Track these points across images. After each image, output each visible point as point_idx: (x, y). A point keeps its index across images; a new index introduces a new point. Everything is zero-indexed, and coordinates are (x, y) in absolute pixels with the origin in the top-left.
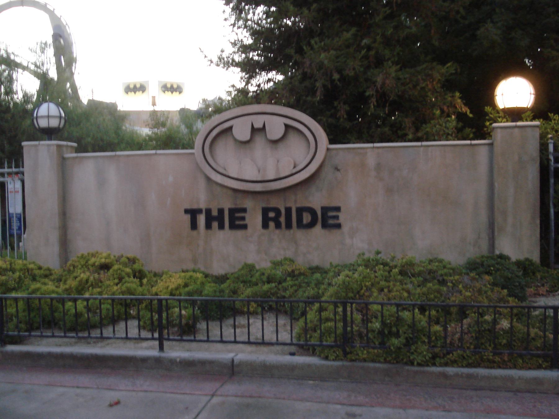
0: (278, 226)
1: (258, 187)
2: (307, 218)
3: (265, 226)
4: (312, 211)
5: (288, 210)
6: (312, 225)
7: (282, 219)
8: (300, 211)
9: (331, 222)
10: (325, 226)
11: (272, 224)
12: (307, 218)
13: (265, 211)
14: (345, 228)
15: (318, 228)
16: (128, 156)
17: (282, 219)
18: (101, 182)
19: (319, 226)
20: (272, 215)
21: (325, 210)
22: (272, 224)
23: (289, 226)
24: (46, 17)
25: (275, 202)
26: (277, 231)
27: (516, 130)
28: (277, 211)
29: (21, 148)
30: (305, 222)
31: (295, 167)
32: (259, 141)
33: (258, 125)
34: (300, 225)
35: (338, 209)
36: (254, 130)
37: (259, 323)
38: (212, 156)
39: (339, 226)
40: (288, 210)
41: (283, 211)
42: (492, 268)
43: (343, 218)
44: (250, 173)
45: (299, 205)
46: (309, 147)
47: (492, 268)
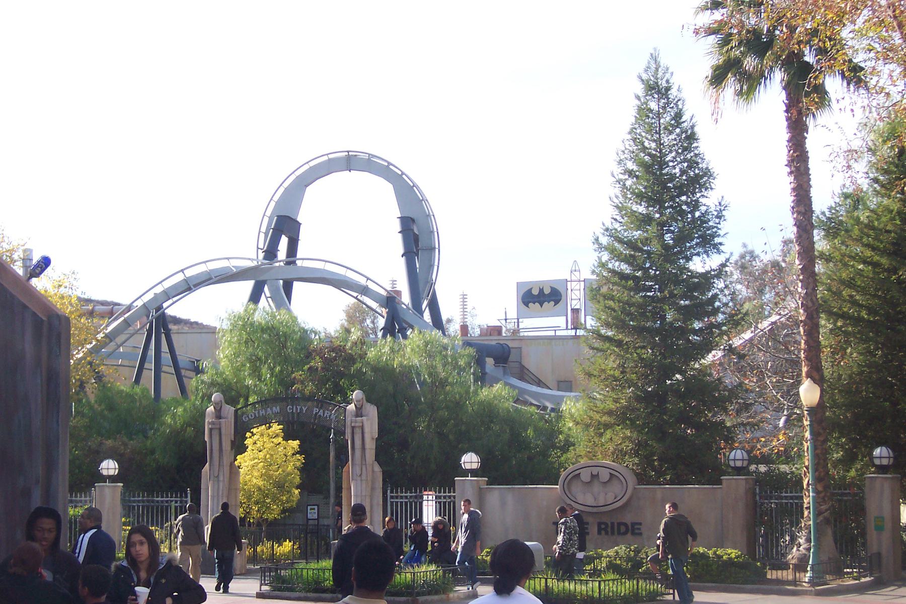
0: (607, 533)
1: (595, 510)
2: (623, 529)
3: (599, 533)
4: (626, 525)
5: (613, 524)
6: (625, 533)
7: (609, 530)
8: (620, 524)
9: (637, 531)
10: (633, 533)
11: (603, 532)
12: (623, 529)
13: (599, 524)
14: (645, 536)
15: (629, 535)
16: (519, 488)
17: (609, 530)
18: (503, 504)
19: (629, 534)
20: (603, 526)
21: (633, 524)
22: (603, 532)
23: (613, 533)
24: (385, 190)
25: (604, 520)
26: (606, 536)
27: (734, 481)
28: (606, 524)
29: (454, 481)
30: (622, 531)
31: (615, 498)
32: (596, 483)
33: (595, 473)
34: (619, 533)
35: (640, 524)
36: (593, 476)
37: (517, 366)
38: (570, 492)
39: (641, 534)
40: (613, 524)
41: (609, 524)
42: (668, 237)
43: (643, 529)
44: (590, 501)
45: (618, 521)
46: (623, 483)
47: (668, 237)
